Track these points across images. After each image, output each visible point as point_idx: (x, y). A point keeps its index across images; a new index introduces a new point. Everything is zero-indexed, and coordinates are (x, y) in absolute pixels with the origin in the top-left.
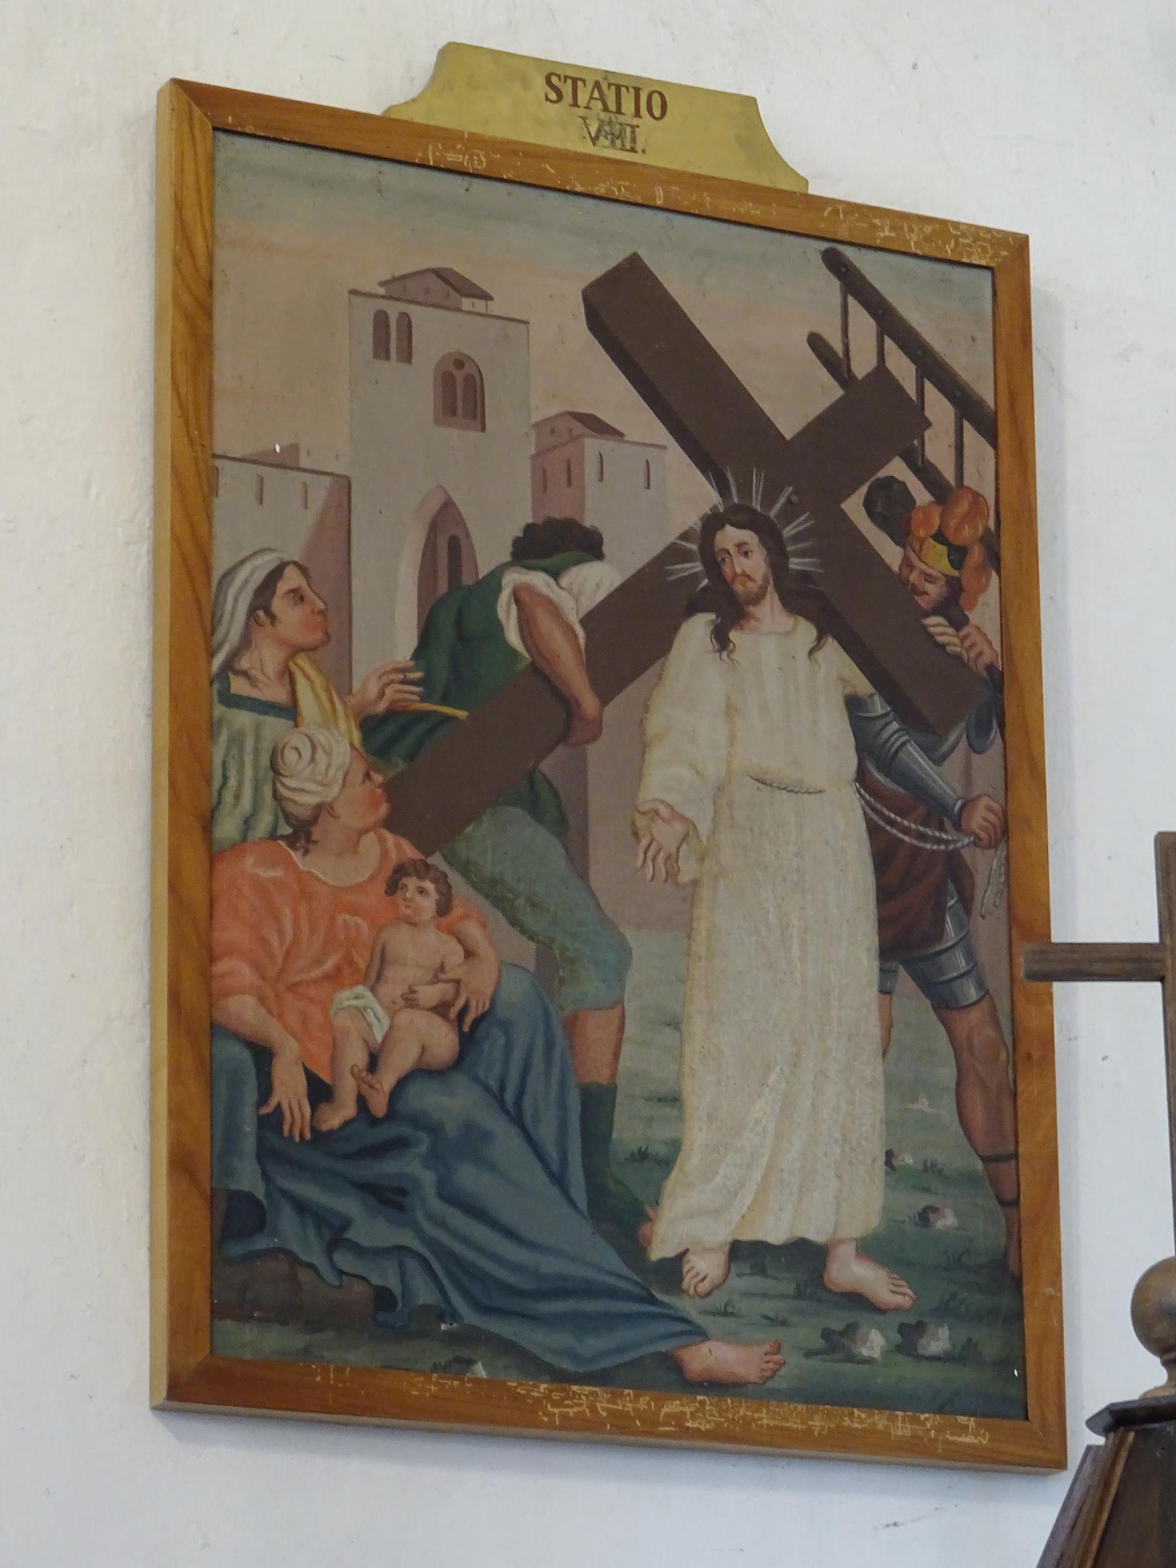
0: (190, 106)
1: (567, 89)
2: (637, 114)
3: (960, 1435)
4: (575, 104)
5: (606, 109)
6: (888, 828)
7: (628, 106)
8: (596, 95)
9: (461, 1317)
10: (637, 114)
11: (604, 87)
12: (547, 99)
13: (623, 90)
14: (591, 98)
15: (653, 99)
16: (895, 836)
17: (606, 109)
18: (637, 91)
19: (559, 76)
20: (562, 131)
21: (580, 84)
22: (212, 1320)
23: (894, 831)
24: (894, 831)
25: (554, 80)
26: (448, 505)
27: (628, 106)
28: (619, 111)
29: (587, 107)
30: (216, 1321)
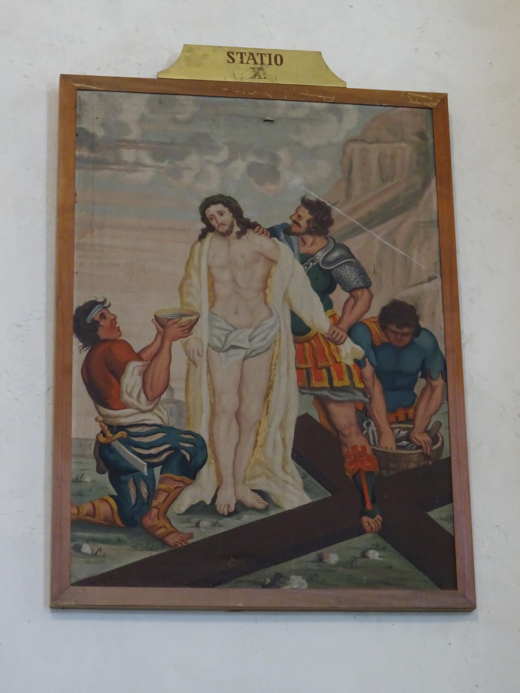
0: (232, 223)
1: (237, 58)
2: (270, 64)
3: (341, 215)
4: (242, 62)
5: (256, 63)
6: (403, 452)
7: (266, 60)
8: (251, 57)
9: (304, 423)
10: (270, 64)
11: (255, 56)
12: (228, 62)
13: (264, 56)
14: (249, 59)
15: (277, 58)
16: (422, 97)
17: (256, 63)
18: (270, 55)
19: (233, 53)
20: (243, 74)
21: (244, 54)
22: (450, 457)
23: (418, 95)
24: (418, 95)
25: (231, 54)
26: (218, 212)
27: (266, 60)
28: (262, 63)
29: (247, 63)
30: (449, 456)
